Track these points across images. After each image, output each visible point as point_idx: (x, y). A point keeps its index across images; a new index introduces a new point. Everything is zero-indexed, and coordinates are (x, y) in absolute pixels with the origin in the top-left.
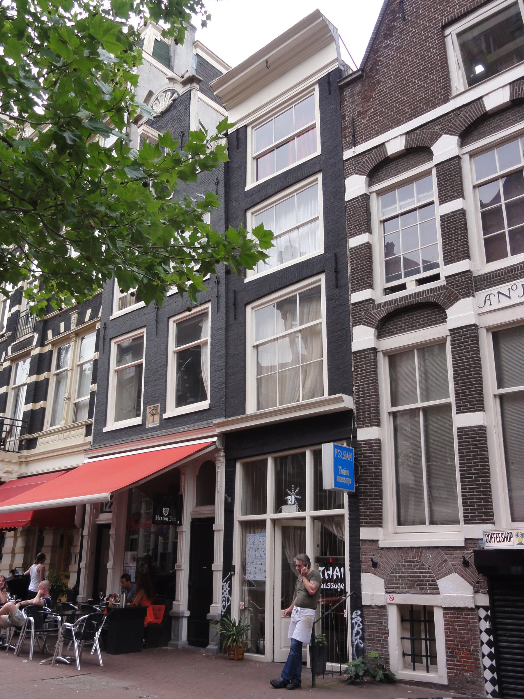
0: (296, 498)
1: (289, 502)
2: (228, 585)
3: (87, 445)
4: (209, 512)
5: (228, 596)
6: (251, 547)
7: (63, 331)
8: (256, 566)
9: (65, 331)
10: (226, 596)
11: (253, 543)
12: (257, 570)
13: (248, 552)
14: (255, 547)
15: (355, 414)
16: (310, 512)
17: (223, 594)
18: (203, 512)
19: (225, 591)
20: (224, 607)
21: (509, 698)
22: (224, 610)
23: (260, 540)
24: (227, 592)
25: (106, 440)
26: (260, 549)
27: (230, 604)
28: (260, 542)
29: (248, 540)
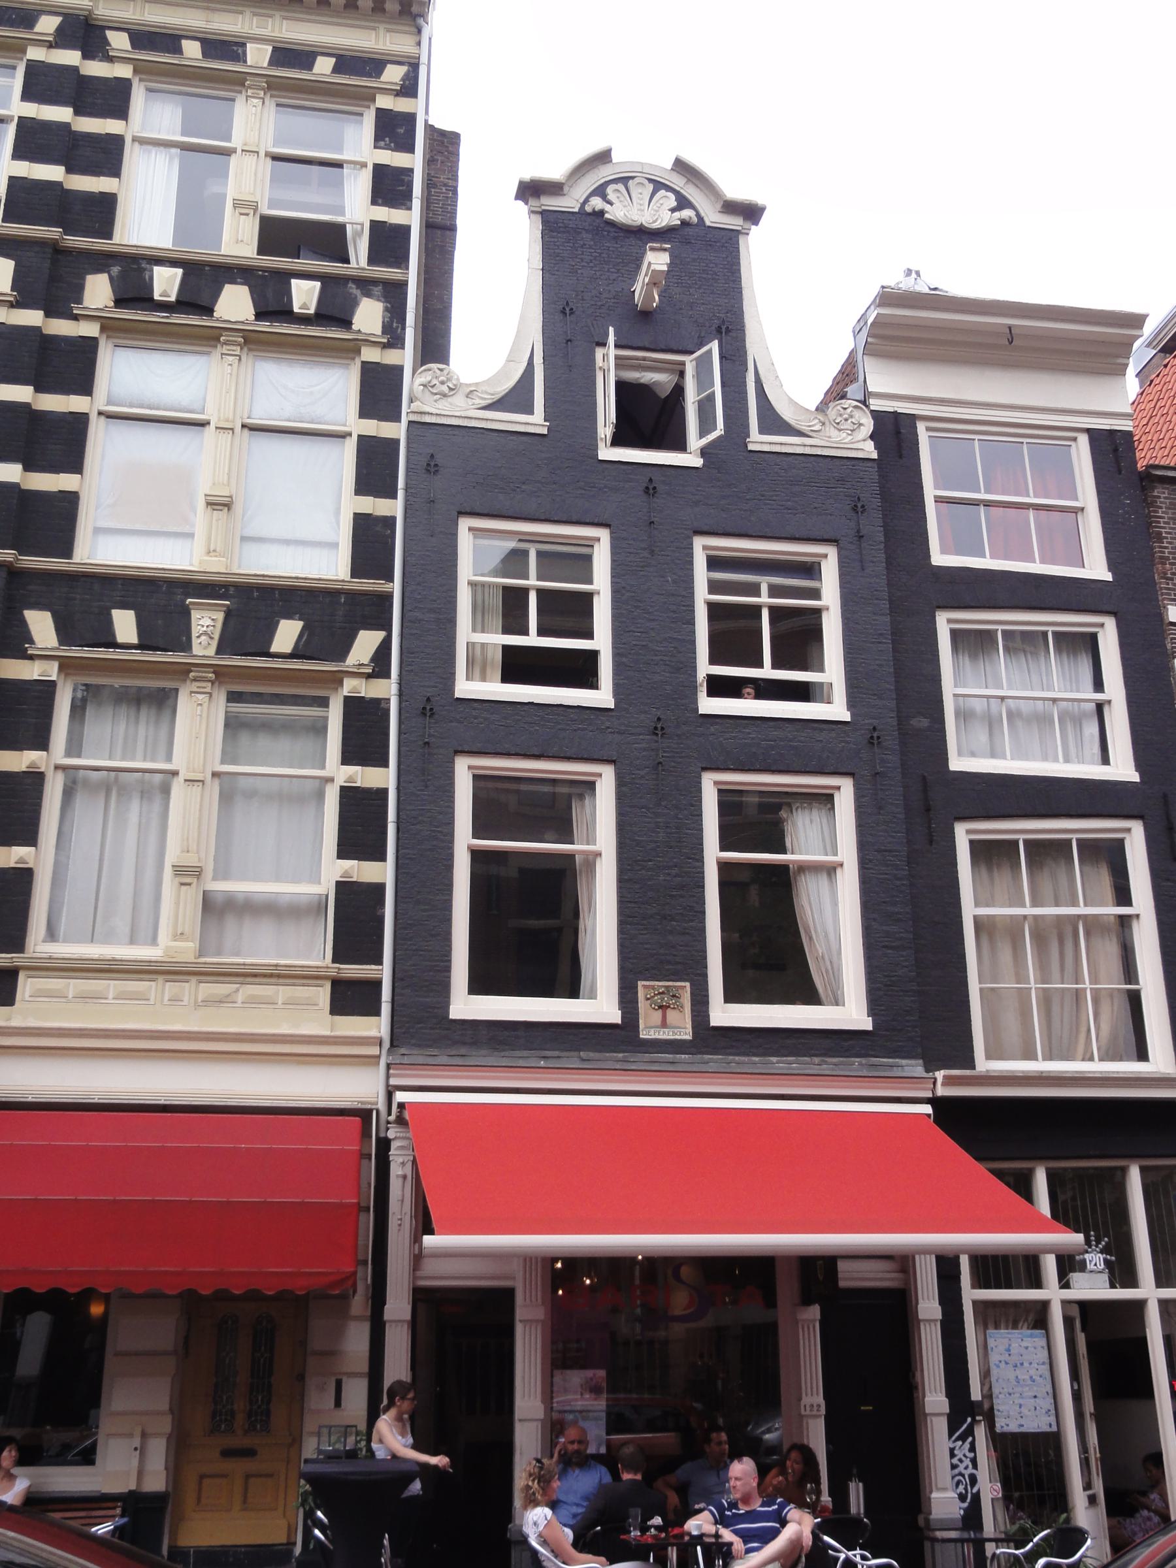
0: (1105, 1260)
1: (1090, 1266)
2: (967, 1445)
3: (373, 1044)
4: (871, 1275)
5: (970, 1470)
6: (1002, 1358)
7: (287, 648)
8: (1021, 1401)
9: (294, 655)
10: (967, 1473)
11: (1008, 1350)
12: (1025, 1411)
13: (994, 1372)
14: (1015, 1359)
15: (187, 993)
16: (1148, 1290)
17: (954, 1467)
18: (855, 1275)
19: (961, 1461)
20: (962, 1498)
21: (1171, 1565)
22: (965, 1505)
23: (1024, 1344)
24: (967, 1462)
25: (464, 1044)
26: (1026, 1364)
27: (979, 1492)
28: (1027, 1348)
29: (991, 1343)
